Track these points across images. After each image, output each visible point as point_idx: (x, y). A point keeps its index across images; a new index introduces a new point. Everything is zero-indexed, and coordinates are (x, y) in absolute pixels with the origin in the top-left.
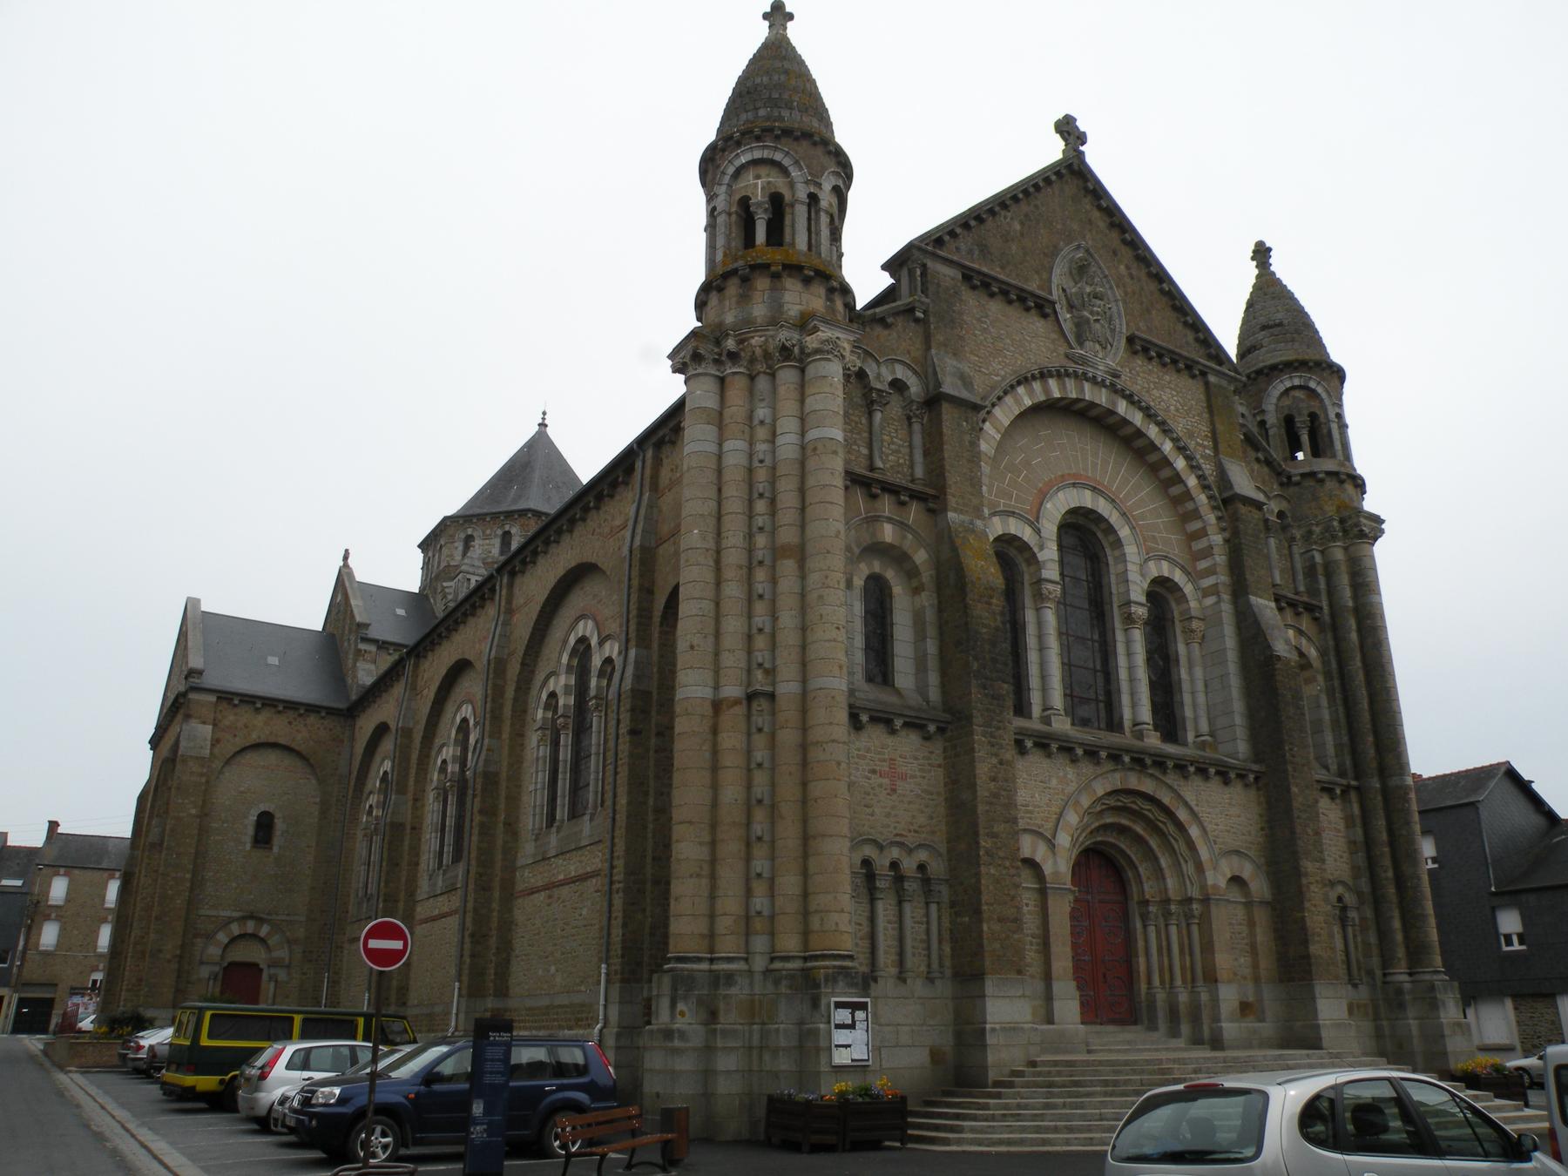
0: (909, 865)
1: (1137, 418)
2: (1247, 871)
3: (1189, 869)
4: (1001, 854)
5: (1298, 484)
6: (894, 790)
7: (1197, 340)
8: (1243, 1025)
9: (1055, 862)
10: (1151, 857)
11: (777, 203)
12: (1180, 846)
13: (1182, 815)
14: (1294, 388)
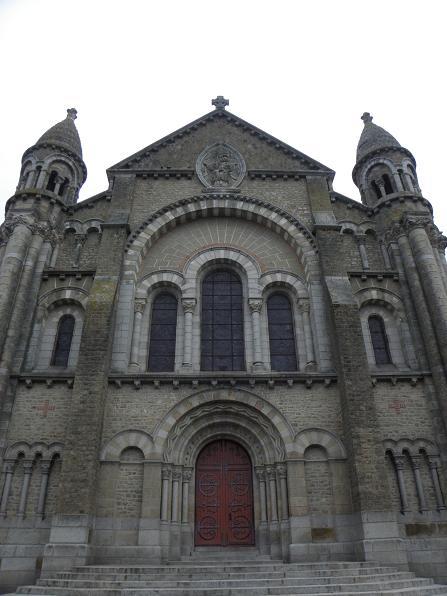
0: (414, 450)
1: (251, 208)
2: (325, 440)
3: (276, 444)
4: (81, 443)
5: (378, 212)
6: (45, 416)
7: (302, 163)
8: (311, 544)
9: (153, 448)
10: (256, 441)
11: (386, 178)
12: (270, 431)
13: (265, 411)
14: (372, 167)
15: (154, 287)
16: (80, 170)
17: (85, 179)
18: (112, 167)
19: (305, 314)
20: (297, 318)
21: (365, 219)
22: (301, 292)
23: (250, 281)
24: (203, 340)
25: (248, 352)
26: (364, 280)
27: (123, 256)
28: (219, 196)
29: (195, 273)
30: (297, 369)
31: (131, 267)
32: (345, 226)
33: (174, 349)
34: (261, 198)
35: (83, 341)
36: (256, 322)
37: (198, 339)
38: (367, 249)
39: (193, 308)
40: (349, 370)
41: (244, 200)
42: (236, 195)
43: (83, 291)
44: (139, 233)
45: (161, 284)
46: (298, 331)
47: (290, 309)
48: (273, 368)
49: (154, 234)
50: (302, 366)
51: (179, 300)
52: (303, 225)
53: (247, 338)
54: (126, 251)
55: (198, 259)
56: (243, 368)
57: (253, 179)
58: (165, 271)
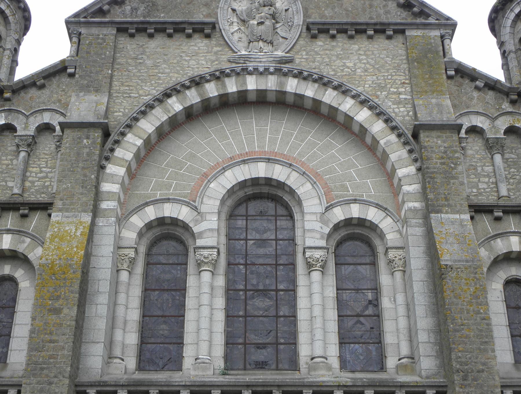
15: (149, 226)
16: (19, 15)
17: (26, 28)
18: (77, 15)
19: (398, 275)
20: (385, 279)
21: (506, 106)
22: (391, 237)
23: (307, 217)
24: (229, 317)
25: (303, 338)
26: (498, 219)
27: (97, 178)
28: (256, 69)
29: (218, 203)
30: (382, 368)
31: (110, 195)
32: (467, 123)
33: (182, 333)
34: (327, 72)
35: (486, 319)
36: (316, 288)
37: (220, 316)
38: (505, 160)
39: (215, 264)
40: (465, 378)
41: (299, 75)
42: (286, 68)
43: (33, 237)
44: (123, 134)
45: (161, 221)
46: (386, 303)
47: (374, 264)
48: (344, 364)
49: (150, 135)
50: (391, 362)
51: (191, 250)
52: (398, 119)
53: (302, 315)
54: (103, 167)
55: (222, 179)
56: (294, 365)
57: (314, 37)
58: (168, 200)
